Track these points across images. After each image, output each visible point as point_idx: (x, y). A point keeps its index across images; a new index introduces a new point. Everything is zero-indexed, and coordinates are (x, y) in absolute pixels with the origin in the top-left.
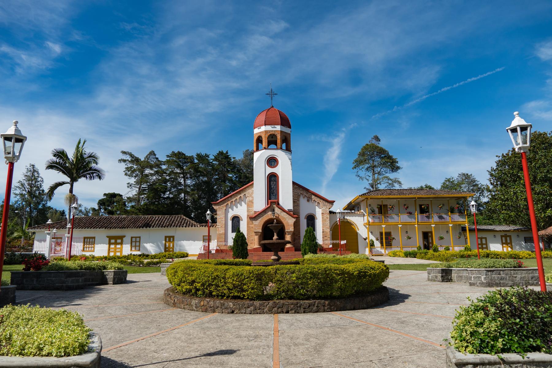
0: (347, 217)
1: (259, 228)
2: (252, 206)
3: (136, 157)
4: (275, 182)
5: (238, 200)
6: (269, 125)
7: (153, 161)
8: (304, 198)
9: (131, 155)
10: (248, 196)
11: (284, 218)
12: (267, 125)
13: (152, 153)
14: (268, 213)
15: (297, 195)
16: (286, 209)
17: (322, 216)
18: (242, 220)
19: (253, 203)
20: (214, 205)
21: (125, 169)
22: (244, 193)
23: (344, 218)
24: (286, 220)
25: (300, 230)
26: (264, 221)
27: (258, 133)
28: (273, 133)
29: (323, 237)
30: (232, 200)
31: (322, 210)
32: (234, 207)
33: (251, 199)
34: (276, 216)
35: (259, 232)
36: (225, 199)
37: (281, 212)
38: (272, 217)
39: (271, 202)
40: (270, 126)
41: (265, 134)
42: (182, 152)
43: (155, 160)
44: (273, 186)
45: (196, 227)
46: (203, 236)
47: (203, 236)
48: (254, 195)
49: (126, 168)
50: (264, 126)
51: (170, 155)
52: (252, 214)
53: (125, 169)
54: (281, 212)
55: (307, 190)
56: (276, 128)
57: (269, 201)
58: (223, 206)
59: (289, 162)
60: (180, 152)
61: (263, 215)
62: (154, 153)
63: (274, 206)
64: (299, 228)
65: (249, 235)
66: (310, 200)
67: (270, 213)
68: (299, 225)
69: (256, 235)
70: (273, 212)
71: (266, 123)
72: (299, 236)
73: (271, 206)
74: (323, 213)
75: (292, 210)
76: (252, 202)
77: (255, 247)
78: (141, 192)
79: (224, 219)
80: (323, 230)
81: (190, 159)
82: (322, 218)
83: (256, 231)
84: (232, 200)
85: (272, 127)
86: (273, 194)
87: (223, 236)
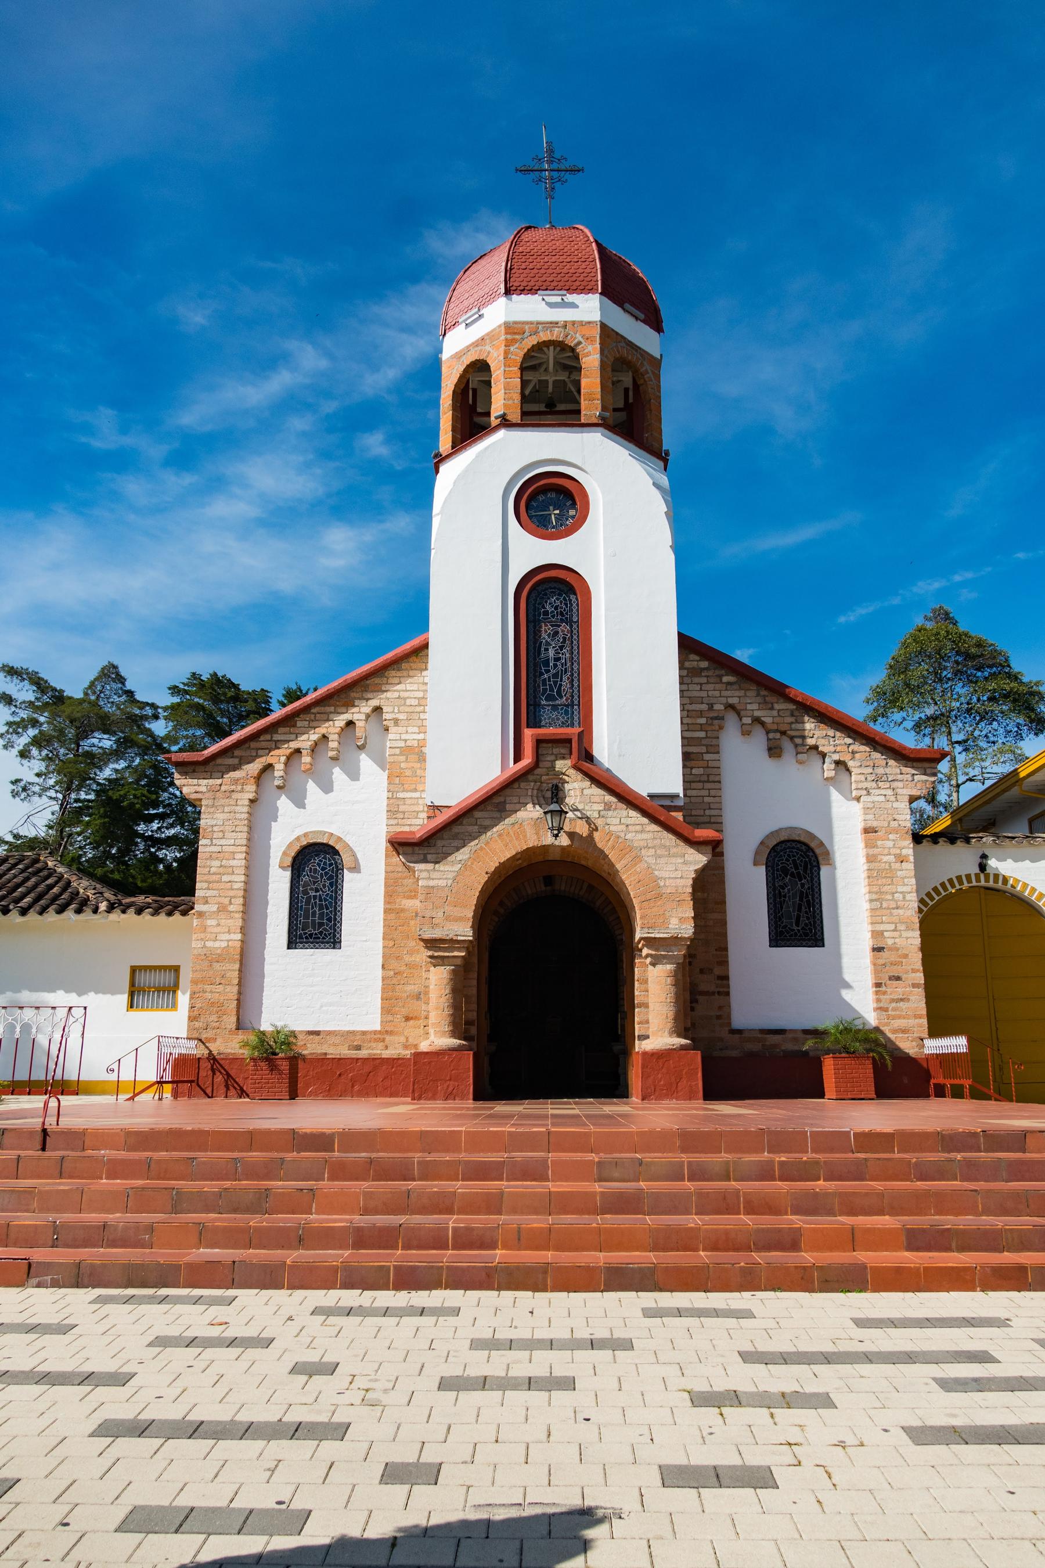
0: (999, 860)
1: (458, 912)
2: (417, 781)
3: (54, 689)
4: (564, 628)
5: (333, 745)
6: (532, 291)
7: (112, 704)
8: (746, 733)
9: (39, 684)
10: (396, 722)
11: (627, 848)
12: (522, 291)
13: (111, 674)
14: (521, 815)
15: (701, 714)
16: (642, 786)
17: (868, 845)
18: (356, 869)
19: (422, 758)
20: (184, 774)
21: (6, 728)
22: (374, 703)
23: (983, 867)
24: (638, 859)
25: (724, 935)
26: (492, 866)
27: (468, 349)
28: (556, 335)
29: (878, 985)
30: (294, 745)
31: (866, 810)
32: (311, 787)
33: (413, 737)
34: (571, 835)
35: (452, 943)
36: (255, 736)
37: (608, 807)
38: (548, 839)
39: (539, 742)
40: (537, 298)
41: (508, 343)
42: (228, 676)
43: (124, 698)
44: (551, 653)
45: (87, 915)
46: (134, 970)
47: (134, 970)
48: (430, 717)
49: (9, 724)
50: (503, 300)
51: (181, 686)
52: (418, 825)
53: (6, 728)
54: (608, 807)
55: (775, 689)
56: (573, 305)
57: (528, 733)
58: (236, 781)
59: (659, 506)
60: (220, 674)
61: (486, 829)
62: (118, 674)
63: (562, 765)
64: (723, 923)
65: (394, 964)
66: (787, 746)
67: (532, 813)
68: (723, 902)
69: (437, 961)
70: (554, 807)
71: (514, 283)
72: (717, 971)
73: (536, 764)
74: (874, 830)
75: (674, 797)
76: (417, 753)
77: (424, 1046)
78: (69, 817)
79: (239, 862)
80: (876, 934)
81: (255, 700)
82: (870, 859)
83: (437, 934)
84: (294, 745)
85: (551, 305)
86: (551, 698)
87: (232, 970)
